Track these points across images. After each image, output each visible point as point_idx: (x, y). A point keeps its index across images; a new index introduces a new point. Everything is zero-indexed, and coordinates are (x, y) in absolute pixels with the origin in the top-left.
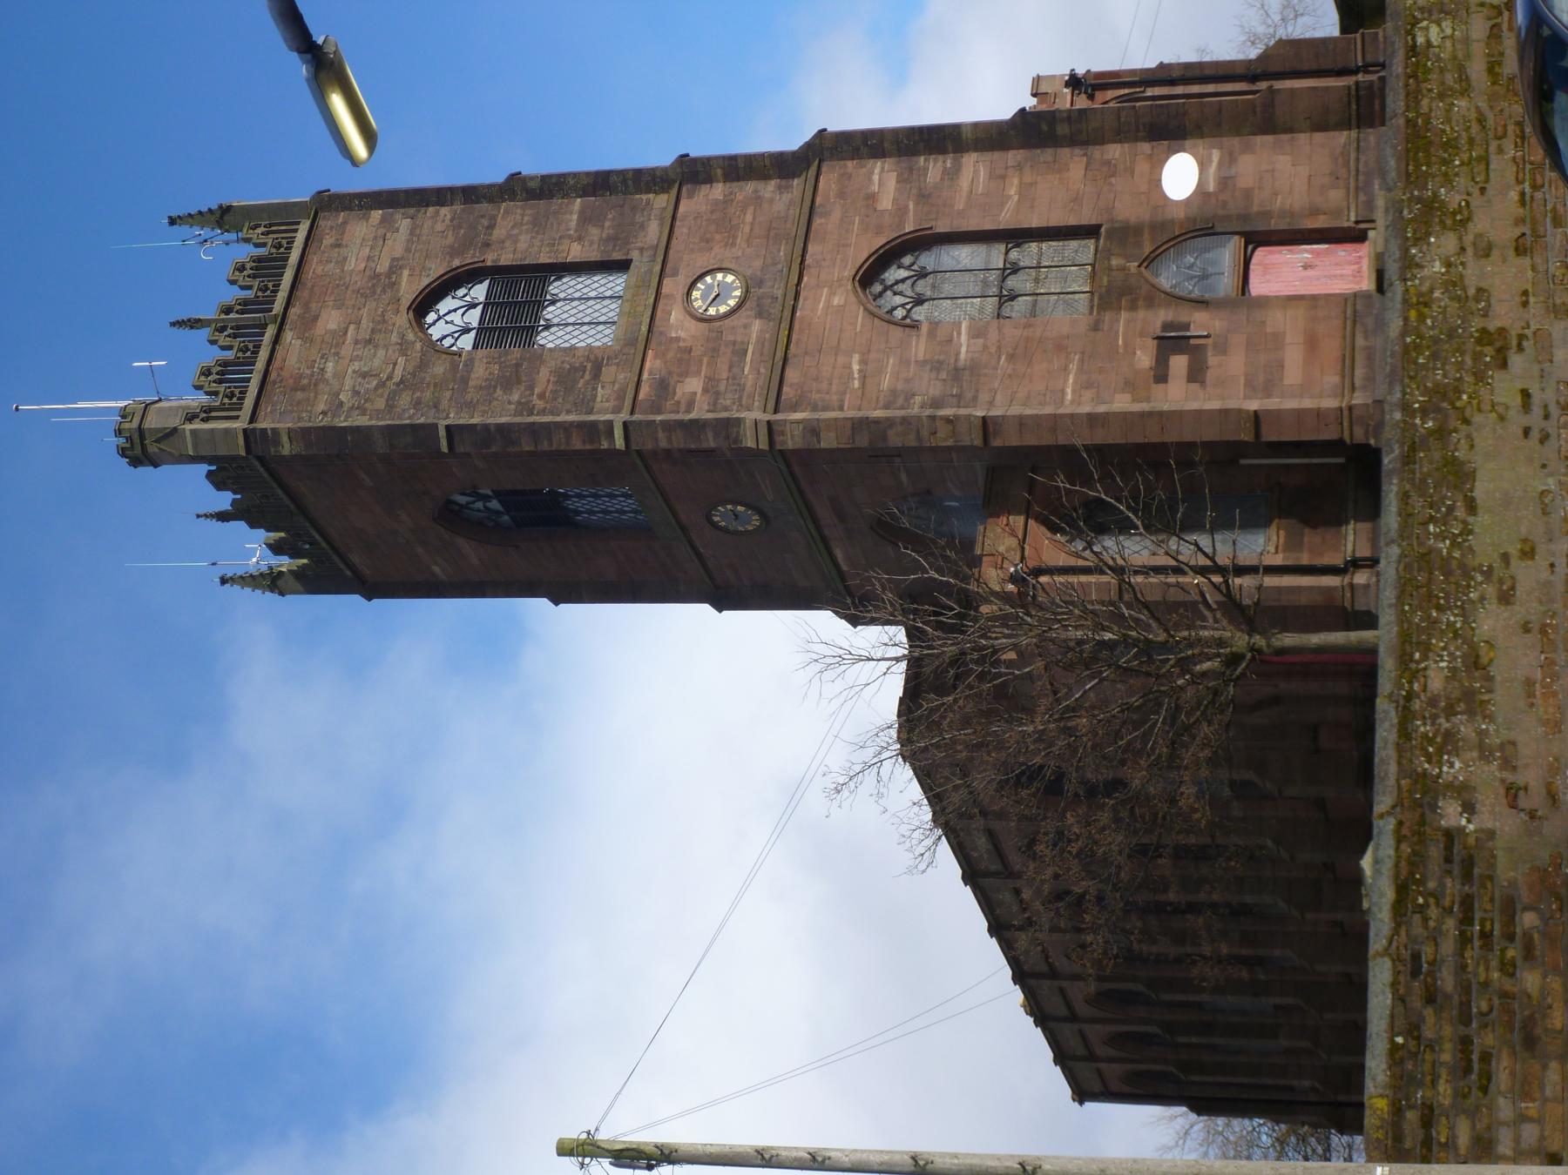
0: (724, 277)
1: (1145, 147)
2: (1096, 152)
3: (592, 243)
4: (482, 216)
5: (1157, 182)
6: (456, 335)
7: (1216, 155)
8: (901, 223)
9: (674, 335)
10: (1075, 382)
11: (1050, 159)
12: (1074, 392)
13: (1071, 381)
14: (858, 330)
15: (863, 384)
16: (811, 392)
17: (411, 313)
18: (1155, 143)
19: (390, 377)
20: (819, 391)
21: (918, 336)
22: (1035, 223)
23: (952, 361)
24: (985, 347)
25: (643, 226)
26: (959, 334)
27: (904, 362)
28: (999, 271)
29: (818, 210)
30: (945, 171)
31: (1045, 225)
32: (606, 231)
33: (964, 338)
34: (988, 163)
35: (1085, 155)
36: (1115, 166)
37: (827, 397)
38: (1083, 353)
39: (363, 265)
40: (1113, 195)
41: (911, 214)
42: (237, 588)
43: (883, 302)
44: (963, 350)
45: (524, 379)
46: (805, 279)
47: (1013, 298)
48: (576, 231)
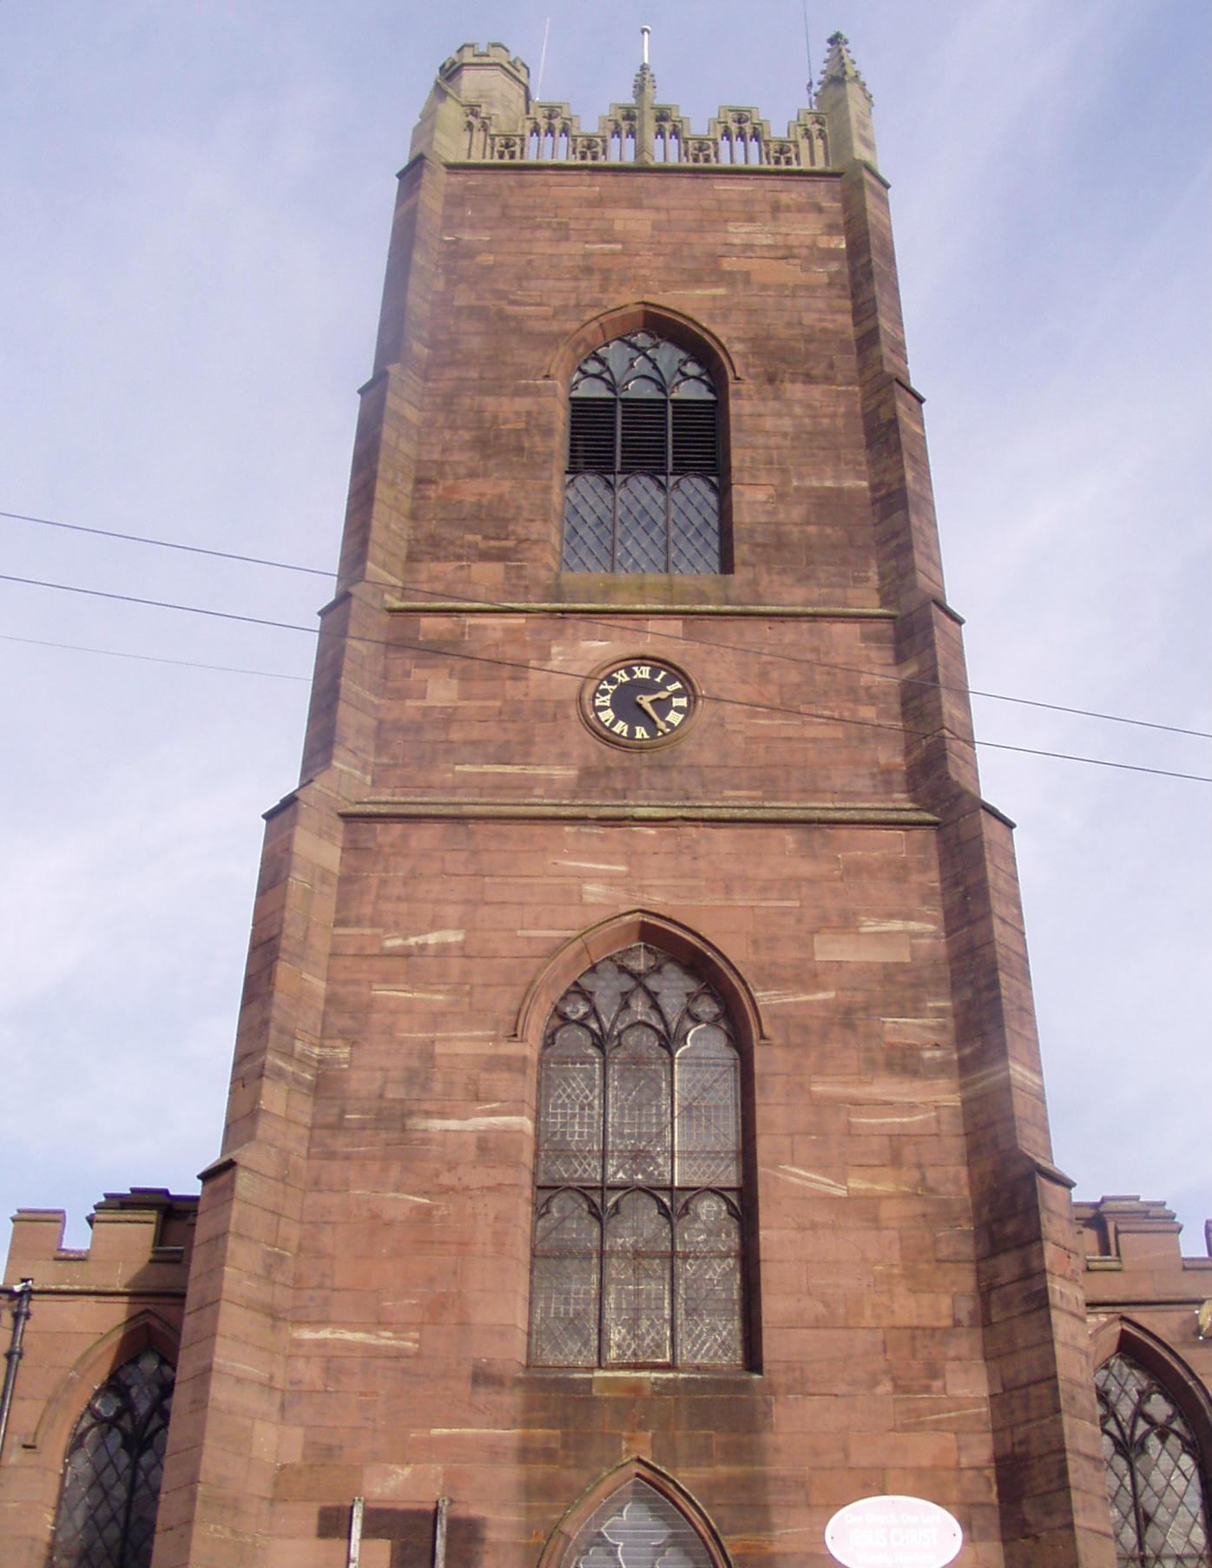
1: (981, 1451)
2: (967, 1344)
3: (774, 512)
4: (831, 366)
5: (874, 1483)
6: (606, 376)
8: (772, 979)
9: (554, 650)
10: (348, 1346)
11: (945, 1251)
13: (348, 1336)
16: (386, 870)
17: (640, 307)
18: (990, 1473)
19: (513, 303)
20: (384, 882)
21: (495, 1039)
22: (768, 1236)
23: (427, 1106)
25: (804, 579)
26: (493, 1113)
27: (436, 1019)
28: (668, 1183)
29: (817, 837)
30: (910, 1052)
31: (763, 1256)
32: (795, 529)
33: (482, 1122)
34: (933, 1128)
35: (957, 1323)
36: (927, 1389)
37: (372, 896)
38: (418, 1355)
40: (841, 1388)
41: (804, 998)
43: (608, 975)
44: (453, 1124)
46: (652, 832)
47: (596, 1213)
48: (797, 489)
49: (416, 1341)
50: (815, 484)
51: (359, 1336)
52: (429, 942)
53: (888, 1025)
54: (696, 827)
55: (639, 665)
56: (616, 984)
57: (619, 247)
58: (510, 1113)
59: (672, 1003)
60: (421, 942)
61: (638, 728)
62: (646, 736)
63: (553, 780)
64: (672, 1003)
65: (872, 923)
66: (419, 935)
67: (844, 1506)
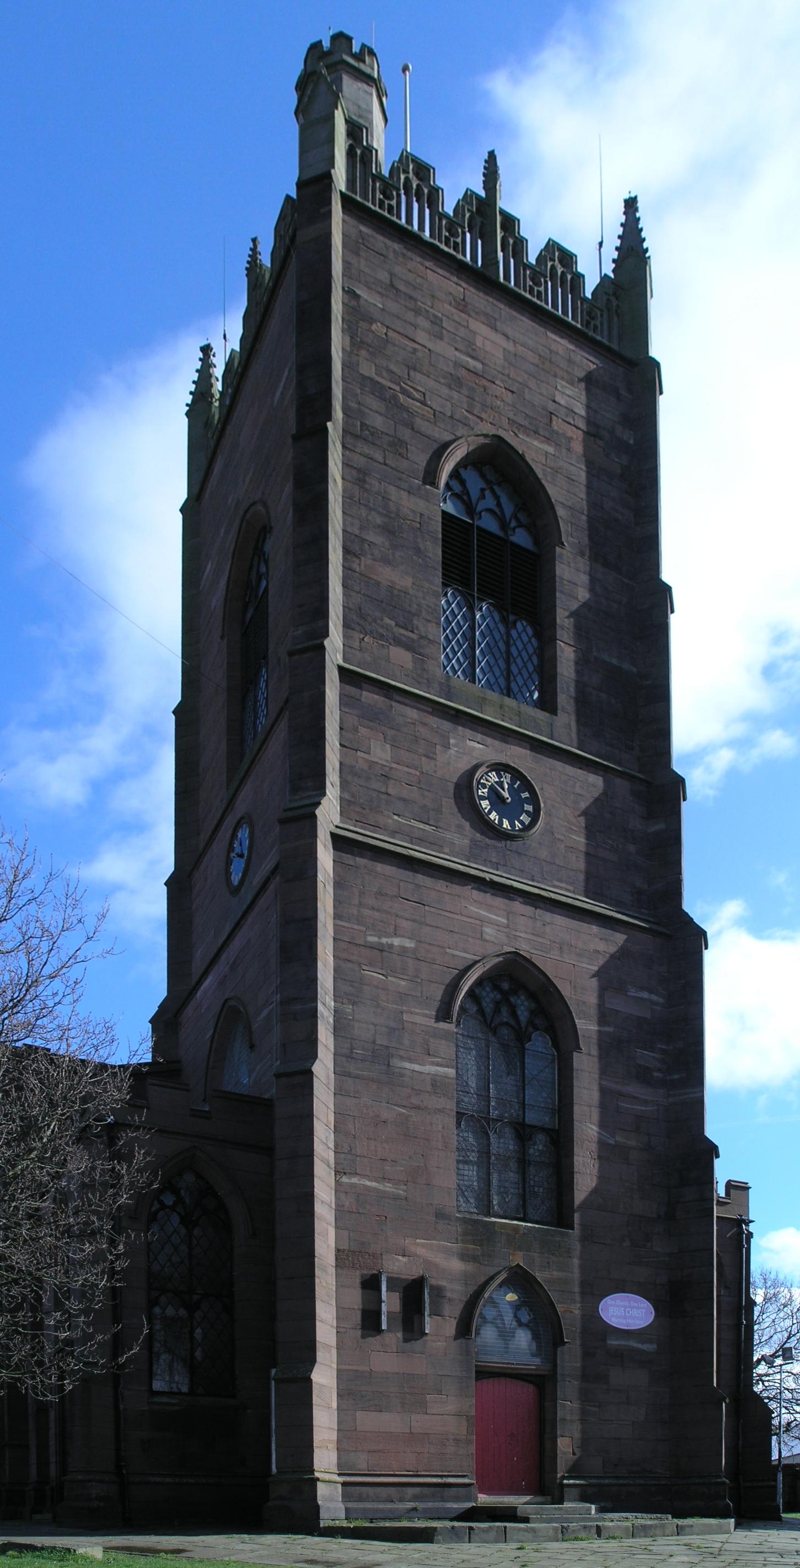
0: (528, 813)
6: (465, 497)
7: (649, 1347)
9: (452, 741)
12: (352, 1186)
13: (368, 1183)
14: (448, 950)
15: (371, 947)
23: (401, 1053)
24: (418, 1092)
26: (438, 1065)
27: (402, 997)
39: (563, 402)
42: (199, 365)
44: (417, 1067)
45: (398, 554)
49: (404, 1191)
50: (606, 658)
51: (374, 1184)
52: (395, 944)
53: (638, 1053)
54: (545, 903)
55: (505, 772)
56: (491, 995)
57: (479, 366)
58: (448, 1067)
59: (523, 1015)
60: (389, 942)
61: (504, 820)
62: (509, 828)
63: (454, 843)
64: (523, 1015)
65: (633, 991)
66: (389, 937)
67: (607, 1296)
